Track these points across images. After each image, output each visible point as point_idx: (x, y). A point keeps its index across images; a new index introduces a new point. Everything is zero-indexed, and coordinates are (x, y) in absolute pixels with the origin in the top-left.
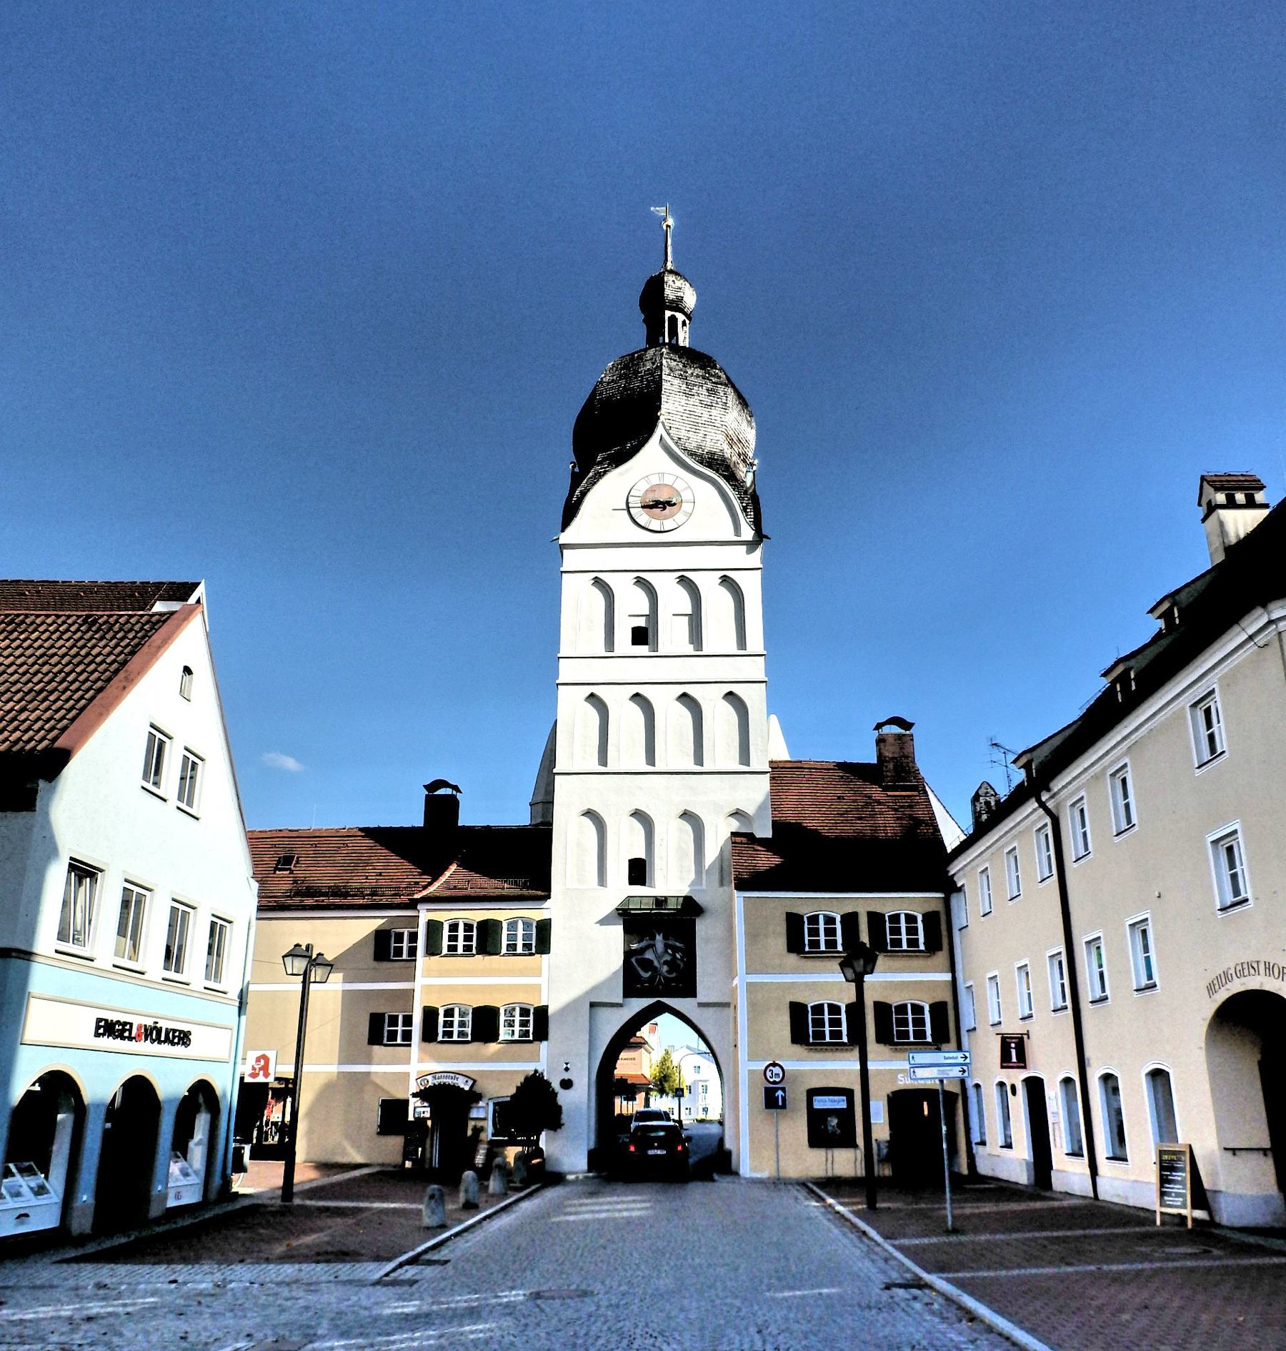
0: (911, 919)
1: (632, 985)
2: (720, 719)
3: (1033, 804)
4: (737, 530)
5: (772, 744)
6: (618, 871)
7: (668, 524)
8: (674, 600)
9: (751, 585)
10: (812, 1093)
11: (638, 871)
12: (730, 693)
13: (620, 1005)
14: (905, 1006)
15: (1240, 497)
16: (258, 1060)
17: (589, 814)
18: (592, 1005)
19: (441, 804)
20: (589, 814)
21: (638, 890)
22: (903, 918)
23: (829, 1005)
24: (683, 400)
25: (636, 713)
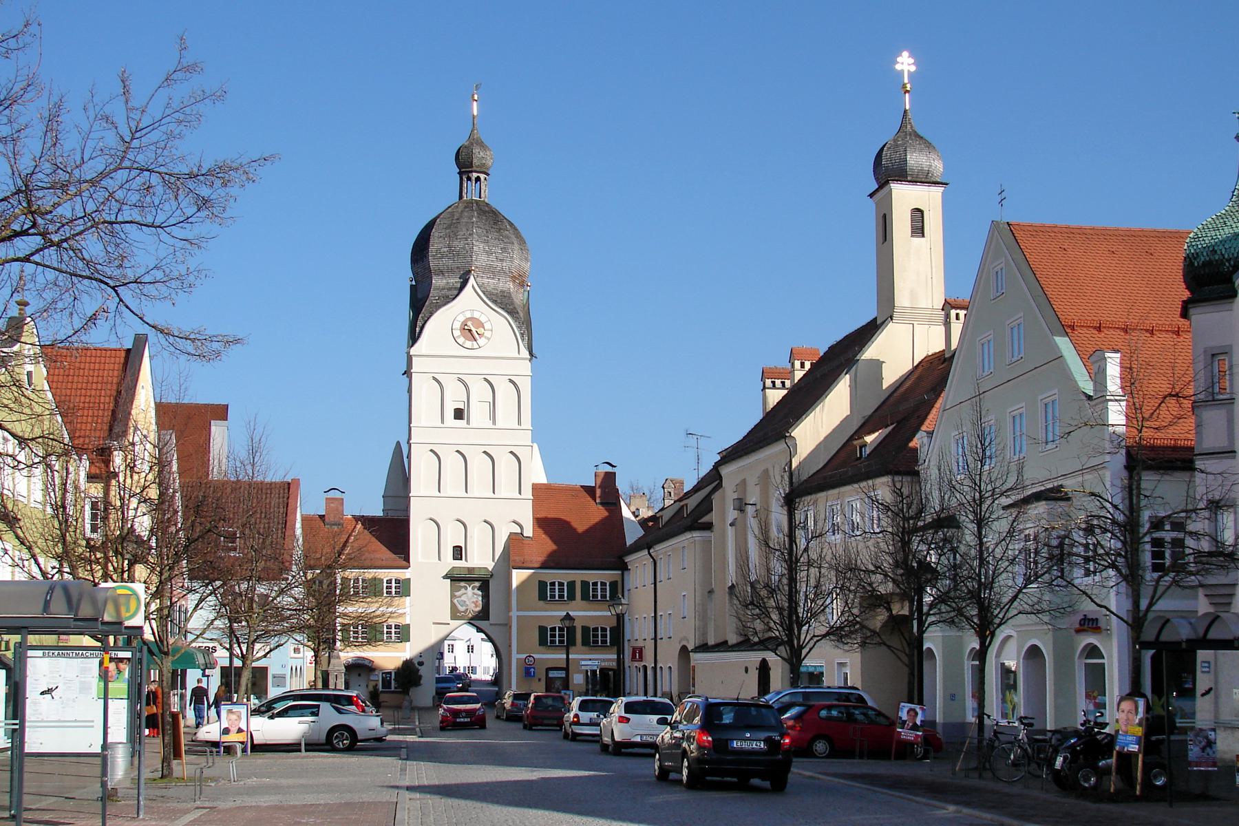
0: (603, 584)
3: (646, 552)
5: (537, 474)
6: (448, 553)
8: (480, 392)
9: (526, 385)
10: (548, 670)
11: (458, 552)
14: (300, 744)
15: (778, 383)
21: (458, 563)
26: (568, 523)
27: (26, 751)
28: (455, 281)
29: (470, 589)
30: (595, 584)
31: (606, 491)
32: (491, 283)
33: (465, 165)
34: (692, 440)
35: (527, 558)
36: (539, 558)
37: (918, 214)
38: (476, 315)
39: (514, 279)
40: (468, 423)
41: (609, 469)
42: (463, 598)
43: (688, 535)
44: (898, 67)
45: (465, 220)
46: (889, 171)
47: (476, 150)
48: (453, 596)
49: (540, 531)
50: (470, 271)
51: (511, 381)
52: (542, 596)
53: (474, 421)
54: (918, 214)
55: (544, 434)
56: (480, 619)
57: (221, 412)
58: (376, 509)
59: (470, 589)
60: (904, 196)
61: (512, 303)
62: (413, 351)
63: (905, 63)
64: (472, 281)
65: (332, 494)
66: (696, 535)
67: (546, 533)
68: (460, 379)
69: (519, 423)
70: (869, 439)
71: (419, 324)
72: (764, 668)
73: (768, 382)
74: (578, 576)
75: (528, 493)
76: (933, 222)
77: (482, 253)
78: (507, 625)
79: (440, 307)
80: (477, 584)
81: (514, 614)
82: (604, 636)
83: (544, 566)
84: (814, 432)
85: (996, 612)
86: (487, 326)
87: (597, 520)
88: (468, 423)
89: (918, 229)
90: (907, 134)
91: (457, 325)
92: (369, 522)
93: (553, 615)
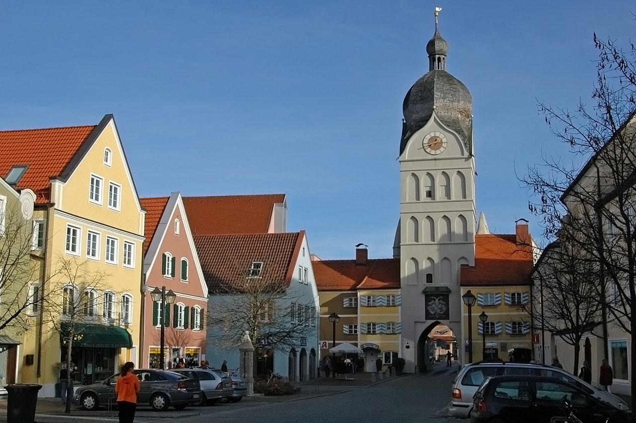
1: (428, 316)
2: (424, 225)
4: (463, 154)
7: (438, 152)
8: (440, 180)
11: (429, 278)
12: (428, 216)
13: (424, 322)
16: (323, 343)
17: (413, 259)
18: (415, 322)
19: (362, 253)
20: (413, 259)
21: (429, 285)
22: (516, 294)
23: (491, 323)
24: (441, 100)
25: (444, 222)
27: (518, 390)
29: (437, 300)
42: (434, 306)
48: (427, 305)
53: (438, 198)
59: (437, 300)
65: (360, 247)
72: (115, 382)
79: (416, 132)
85: (628, 286)
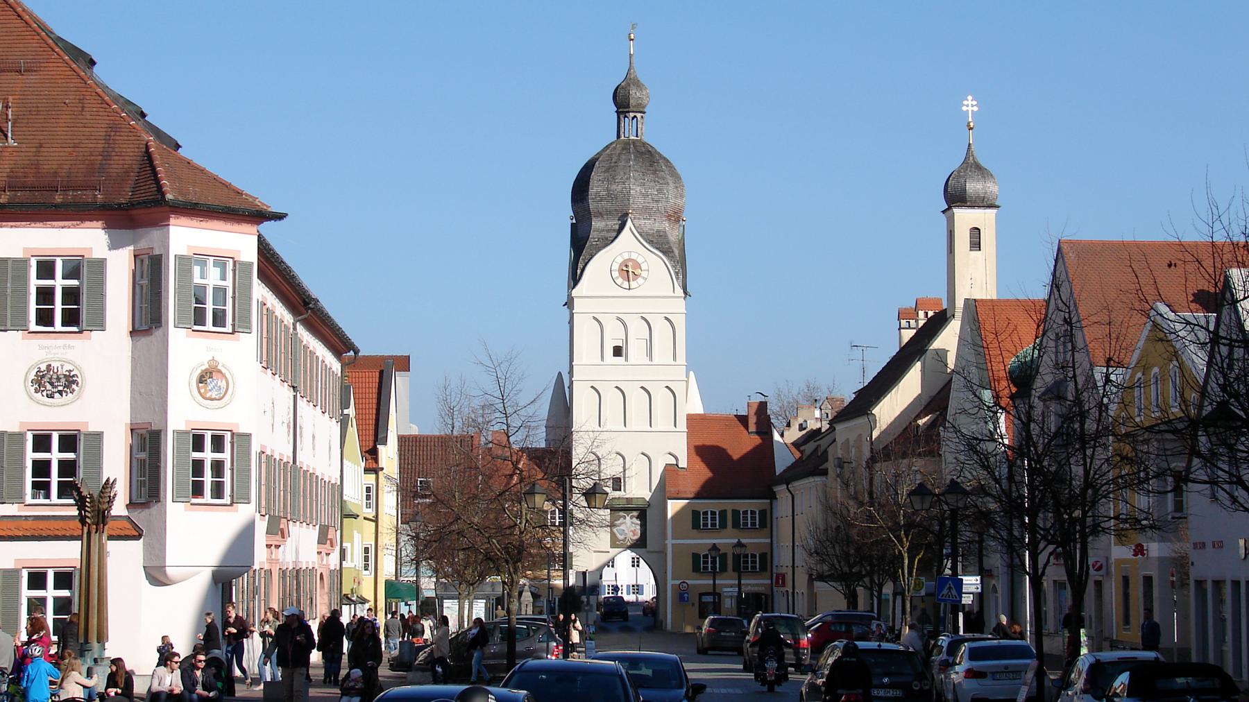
8: (637, 330)
10: (701, 595)
26: (724, 451)
28: (615, 224)
30: (745, 512)
31: (762, 420)
32: (649, 225)
33: (623, 103)
34: (858, 352)
35: (681, 489)
36: (693, 487)
37: (976, 232)
38: (634, 256)
39: (669, 217)
40: (626, 360)
41: (763, 399)
42: (622, 527)
43: (811, 479)
44: (964, 108)
45: (623, 163)
46: (956, 197)
47: (633, 92)
49: (698, 459)
50: (627, 214)
51: (666, 318)
52: (696, 526)
54: (976, 232)
55: (699, 360)
56: (639, 545)
57: (403, 363)
58: (539, 441)
60: (965, 218)
61: (668, 243)
62: (574, 293)
63: (970, 105)
64: (629, 223)
66: (818, 479)
67: (704, 460)
68: (619, 319)
69: (675, 359)
70: (921, 422)
71: (580, 266)
73: (904, 323)
74: (729, 504)
75: (682, 425)
76: (988, 239)
77: (637, 190)
78: (662, 552)
80: (635, 513)
81: (670, 542)
82: (754, 562)
83: (698, 496)
84: (889, 410)
86: (644, 266)
87: (749, 448)
88: (626, 360)
89: (976, 244)
90: (972, 166)
91: (616, 267)
92: (537, 456)
93: (703, 542)
